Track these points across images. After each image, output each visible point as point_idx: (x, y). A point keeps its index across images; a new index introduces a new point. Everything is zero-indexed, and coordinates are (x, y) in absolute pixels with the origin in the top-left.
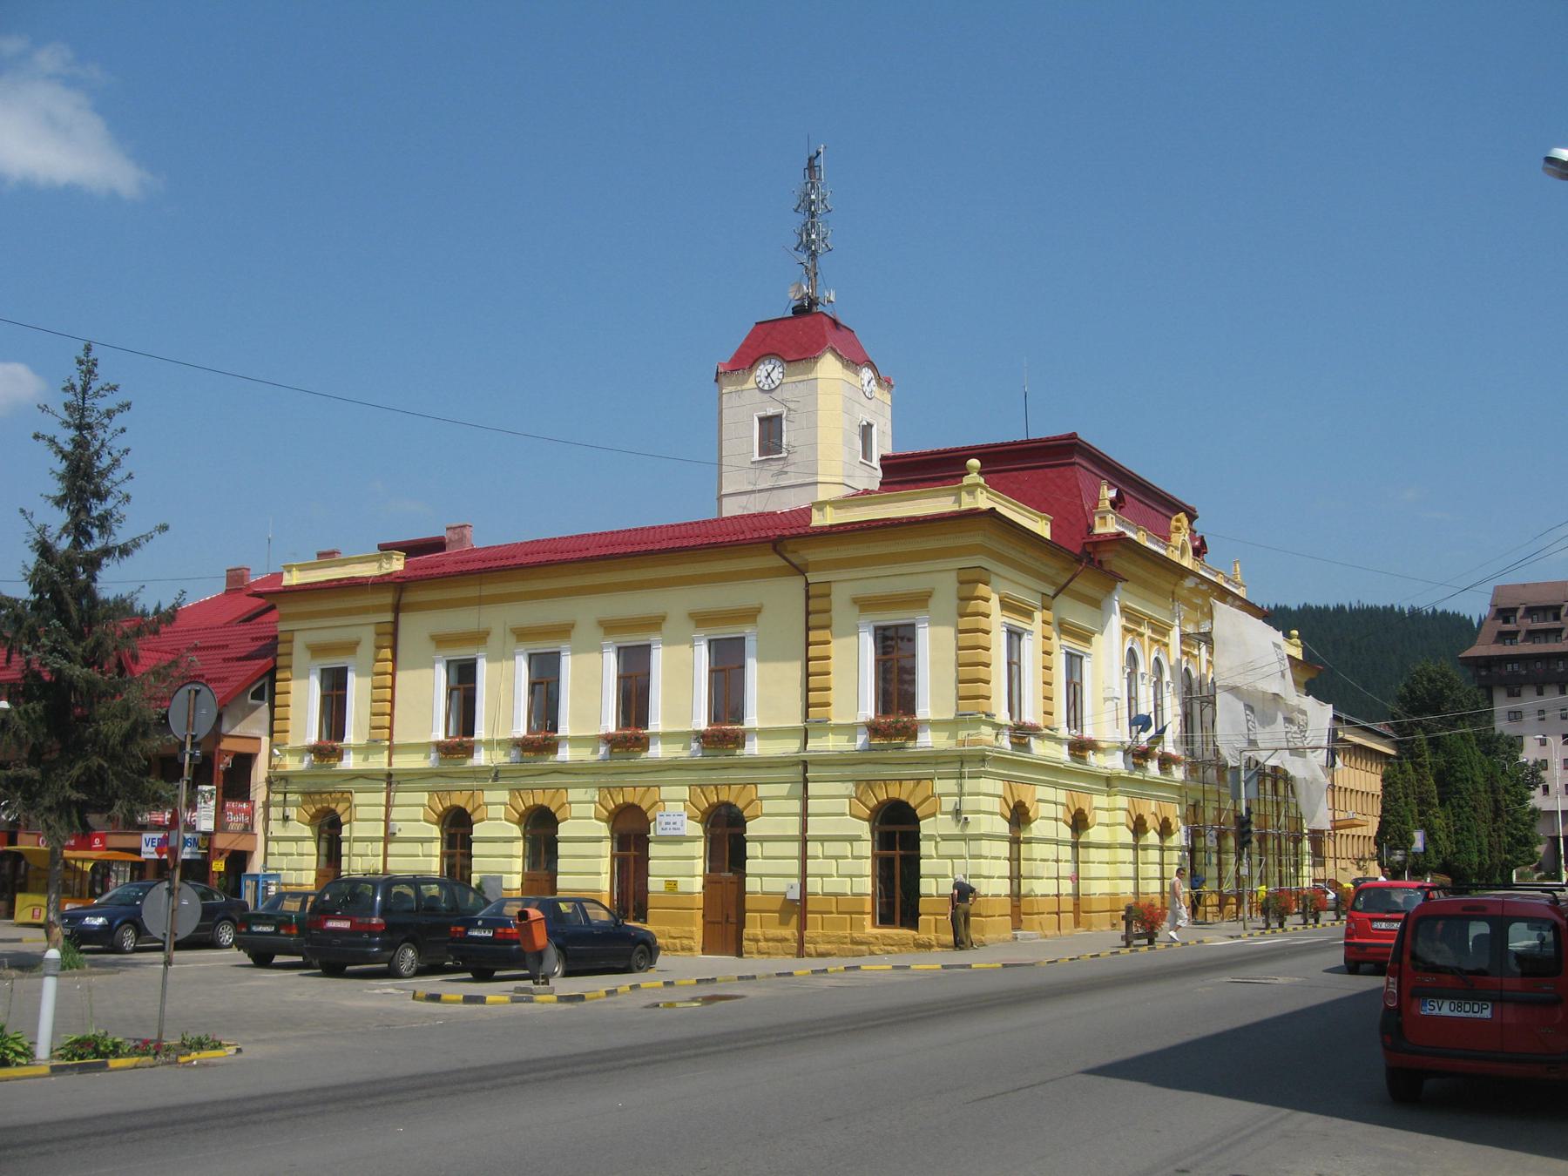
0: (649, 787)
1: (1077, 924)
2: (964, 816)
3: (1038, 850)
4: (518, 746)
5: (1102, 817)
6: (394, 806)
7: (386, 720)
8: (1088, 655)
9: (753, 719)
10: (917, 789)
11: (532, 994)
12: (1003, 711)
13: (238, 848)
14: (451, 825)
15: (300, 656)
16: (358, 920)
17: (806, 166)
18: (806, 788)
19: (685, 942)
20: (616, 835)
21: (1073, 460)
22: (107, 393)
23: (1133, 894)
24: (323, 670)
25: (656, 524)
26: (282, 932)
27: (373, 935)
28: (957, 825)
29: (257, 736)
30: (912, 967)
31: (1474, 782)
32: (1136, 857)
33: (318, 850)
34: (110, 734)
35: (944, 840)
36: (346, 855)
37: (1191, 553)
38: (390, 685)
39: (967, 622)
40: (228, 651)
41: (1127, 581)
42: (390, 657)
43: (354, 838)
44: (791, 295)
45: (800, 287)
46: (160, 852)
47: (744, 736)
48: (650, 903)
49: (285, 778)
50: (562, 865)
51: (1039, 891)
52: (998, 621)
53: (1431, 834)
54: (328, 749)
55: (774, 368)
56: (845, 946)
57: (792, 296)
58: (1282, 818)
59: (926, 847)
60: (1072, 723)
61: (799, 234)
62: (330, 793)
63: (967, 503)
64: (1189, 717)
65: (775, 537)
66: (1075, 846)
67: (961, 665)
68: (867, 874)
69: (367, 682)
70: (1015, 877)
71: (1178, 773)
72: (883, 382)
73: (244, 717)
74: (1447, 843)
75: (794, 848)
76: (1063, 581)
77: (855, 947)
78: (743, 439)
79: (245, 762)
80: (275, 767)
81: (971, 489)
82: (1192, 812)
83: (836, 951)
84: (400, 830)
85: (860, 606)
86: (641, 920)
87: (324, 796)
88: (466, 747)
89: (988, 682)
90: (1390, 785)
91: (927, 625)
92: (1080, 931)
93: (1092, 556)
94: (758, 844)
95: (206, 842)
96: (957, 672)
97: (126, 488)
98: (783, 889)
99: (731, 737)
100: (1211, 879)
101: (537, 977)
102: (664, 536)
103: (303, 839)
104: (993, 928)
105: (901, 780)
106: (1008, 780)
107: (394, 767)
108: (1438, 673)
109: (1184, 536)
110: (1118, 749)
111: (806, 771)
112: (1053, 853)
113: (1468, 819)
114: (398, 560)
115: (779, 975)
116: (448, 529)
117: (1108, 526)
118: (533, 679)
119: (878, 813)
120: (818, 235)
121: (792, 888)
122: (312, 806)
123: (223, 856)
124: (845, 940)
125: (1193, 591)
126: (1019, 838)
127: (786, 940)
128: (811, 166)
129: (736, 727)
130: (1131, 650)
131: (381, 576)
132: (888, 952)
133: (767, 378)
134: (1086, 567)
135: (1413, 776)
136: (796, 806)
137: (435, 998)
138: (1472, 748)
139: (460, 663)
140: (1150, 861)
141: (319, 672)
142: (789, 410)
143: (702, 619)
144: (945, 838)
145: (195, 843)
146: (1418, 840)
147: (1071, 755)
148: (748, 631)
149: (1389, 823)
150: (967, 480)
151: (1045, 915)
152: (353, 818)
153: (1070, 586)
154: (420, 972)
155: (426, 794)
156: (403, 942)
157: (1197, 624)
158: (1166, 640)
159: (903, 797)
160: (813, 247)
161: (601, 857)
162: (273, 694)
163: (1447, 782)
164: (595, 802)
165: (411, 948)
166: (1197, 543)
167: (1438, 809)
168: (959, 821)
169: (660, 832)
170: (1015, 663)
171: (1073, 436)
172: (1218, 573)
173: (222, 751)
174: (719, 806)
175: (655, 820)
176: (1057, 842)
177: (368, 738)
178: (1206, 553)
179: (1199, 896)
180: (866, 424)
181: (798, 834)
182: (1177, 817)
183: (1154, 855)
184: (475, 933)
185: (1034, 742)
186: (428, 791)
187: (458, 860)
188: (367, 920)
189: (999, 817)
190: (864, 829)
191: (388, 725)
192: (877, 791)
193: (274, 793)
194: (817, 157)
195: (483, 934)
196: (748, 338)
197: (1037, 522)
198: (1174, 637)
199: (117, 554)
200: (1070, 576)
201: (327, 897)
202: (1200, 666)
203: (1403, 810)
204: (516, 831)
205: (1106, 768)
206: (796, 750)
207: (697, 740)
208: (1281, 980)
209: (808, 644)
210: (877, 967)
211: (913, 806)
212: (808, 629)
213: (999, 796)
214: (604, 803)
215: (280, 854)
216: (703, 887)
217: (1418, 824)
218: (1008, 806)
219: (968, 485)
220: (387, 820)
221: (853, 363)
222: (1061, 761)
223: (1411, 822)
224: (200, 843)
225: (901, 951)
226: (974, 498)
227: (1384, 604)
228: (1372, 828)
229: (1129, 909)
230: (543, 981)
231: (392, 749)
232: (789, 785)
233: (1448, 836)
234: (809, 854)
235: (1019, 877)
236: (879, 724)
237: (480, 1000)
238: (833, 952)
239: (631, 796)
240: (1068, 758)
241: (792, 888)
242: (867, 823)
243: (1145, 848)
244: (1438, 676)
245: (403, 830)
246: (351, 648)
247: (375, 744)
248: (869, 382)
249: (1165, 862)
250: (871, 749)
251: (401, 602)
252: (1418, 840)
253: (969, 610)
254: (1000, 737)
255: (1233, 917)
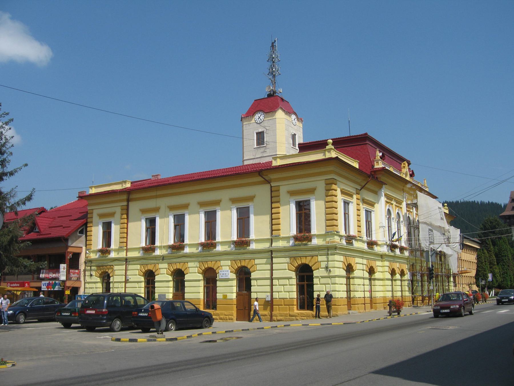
0: (216, 261)
1: (371, 308)
2: (329, 269)
3: (357, 281)
4: (170, 247)
5: (380, 269)
6: (129, 270)
7: (125, 240)
8: (373, 211)
9: (253, 236)
10: (312, 260)
11: (156, 338)
12: (343, 231)
13: (75, 286)
14: (148, 277)
15: (95, 218)
16: (98, 310)
17: (271, 46)
18: (272, 260)
19: (230, 317)
20: (205, 279)
21: (366, 142)
22: (5, 116)
23: (391, 296)
24: (103, 223)
25: (218, 169)
26: (73, 315)
27: (103, 315)
28: (327, 272)
29: (81, 246)
30: (310, 325)
31: (508, 257)
32: (392, 283)
33: (103, 286)
34: (3, 241)
35: (322, 278)
36: (112, 288)
37: (409, 176)
38: (126, 227)
39: (329, 199)
40: (71, 217)
41: (387, 184)
42: (126, 218)
43: (114, 282)
44: (267, 90)
45: (269, 88)
46: (48, 288)
47: (250, 242)
48: (218, 303)
49: (91, 261)
50: (186, 290)
51: (357, 296)
52: (340, 198)
53: (494, 275)
54: (105, 251)
55: (261, 115)
56: (287, 317)
57: (267, 90)
58: (443, 269)
59: (316, 281)
60: (368, 236)
61: (269, 69)
62: (106, 266)
63: (328, 155)
64: (410, 233)
65: (259, 170)
66: (370, 280)
67: (327, 214)
68: (295, 291)
69: (118, 227)
70: (349, 291)
71: (407, 253)
72: (299, 119)
73: (76, 240)
74: (500, 278)
75: (268, 282)
76: (363, 184)
77: (291, 318)
78: (250, 140)
79: (76, 256)
80: (87, 257)
81: (329, 150)
82: (412, 267)
83: (284, 319)
84: (130, 278)
85: (290, 194)
86: (215, 309)
87: (104, 267)
88: (152, 249)
89: (337, 220)
90: (480, 258)
91: (314, 200)
92: (373, 310)
93: (374, 176)
94: (255, 281)
95: (63, 284)
96: (326, 217)
97: (10, 150)
98: (264, 297)
99: (245, 243)
100: (419, 291)
101: (159, 331)
102: (221, 172)
103: (97, 282)
104: (341, 310)
105: (306, 257)
106: (345, 256)
107: (128, 256)
108: (494, 220)
109: (407, 169)
110: (385, 244)
111: (272, 254)
112: (362, 282)
113: (506, 269)
114: (128, 183)
115: (258, 328)
116: (152, 176)
117: (379, 165)
118: (176, 224)
119: (298, 269)
120: (275, 69)
121: (268, 296)
122: (100, 271)
123: (69, 289)
124: (287, 315)
125: (410, 189)
126: (350, 277)
127: (266, 315)
128: (273, 46)
129: (247, 239)
130: (389, 210)
131: (123, 189)
132: (303, 319)
133: (259, 119)
134: (372, 179)
135: (487, 255)
136: (268, 267)
137: (118, 340)
138: (507, 245)
139: (150, 219)
140: (397, 285)
141: (102, 224)
142: (267, 129)
143: (234, 201)
144: (323, 277)
145: (60, 285)
146: (490, 277)
147: (368, 247)
148: (251, 204)
149: (480, 271)
150: (327, 147)
151: (360, 305)
152: (114, 275)
153: (365, 186)
154: (122, 330)
155: (139, 265)
156: (116, 318)
157: (412, 200)
158: (401, 206)
159: (307, 263)
160: (274, 73)
161: (200, 287)
162: (86, 232)
163: (499, 257)
164: (198, 267)
165: (119, 321)
166: (411, 173)
167: (496, 266)
168: (327, 271)
169: (220, 277)
170: (347, 214)
171: (366, 134)
172: (419, 183)
173: (68, 252)
174: (242, 267)
175: (219, 273)
176: (364, 278)
177: (119, 246)
178: (414, 176)
179: (415, 297)
180: (293, 134)
181: (270, 277)
182: (406, 269)
183: (399, 283)
184: (141, 314)
185: (354, 242)
186: (140, 265)
187: (151, 289)
188: (101, 310)
189: (388, 273)
190: (293, 275)
191: (125, 241)
192: (297, 261)
193: (87, 266)
194: (275, 42)
195: (144, 315)
196: (252, 105)
197: (354, 163)
198: (404, 205)
199: (8, 175)
200: (366, 183)
201: (87, 302)
202: (413, 215)
203: (484, 266)
204: (170, 278)
205: (380, 252)
206: (268, 247)
207: (233, 244)
208: (451, 328)
209: (272, 208)
210: (296, 325)
211: (311, 266)
212: (272, 203)
213: (342, 262)
214: (201, 267)
215: (89, 288)
216: (236, 297)
217: (490, 271)
218: (345, 265)
219: (328, 149)
220: (126, 275)
221: (289, 113)
222: (364, 249)
223: (487, 271)
224: (61, 285)
225: (307, 319)
226: (330, 154)
227: (472, 200)
228: (473, 273)
229: (390, 302)
230: (161, 333)
231: (127, 250)
232: (266, 259)
233: (500, 276)
234: (273, 284)
235: (350, 291)
236: (298, 236)
237: (135, 340)
238: (283, 320)
239: (210, 265)
240: (367, 248)
241: (268, 296)
242: (294, 272)
243: (395, 280)
244: (494, 221)
245: (131, 278)
246: (112, 215)
247: (121, 248)
248: (294, 120)
249: (403, 285)
250: (295, 245)
251: (129, 198)
252: (490, 277)
253: (329, 194)
254: (342, 240)
255: (427, 305)
